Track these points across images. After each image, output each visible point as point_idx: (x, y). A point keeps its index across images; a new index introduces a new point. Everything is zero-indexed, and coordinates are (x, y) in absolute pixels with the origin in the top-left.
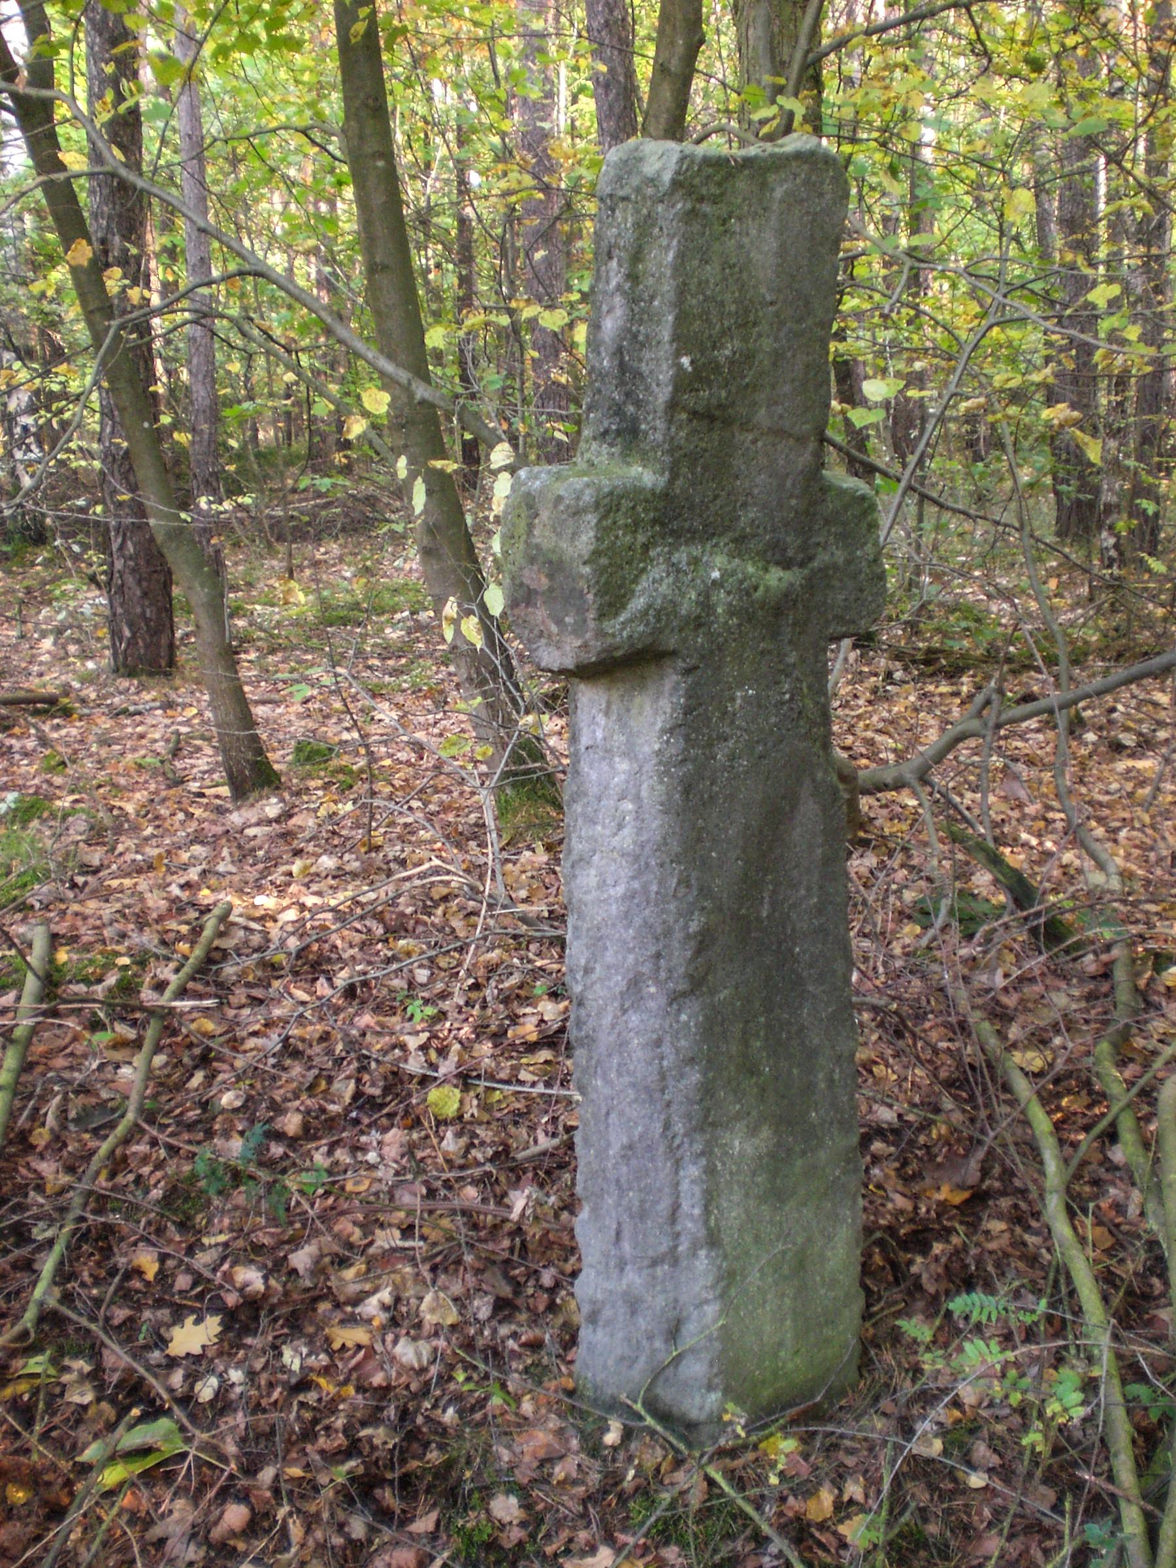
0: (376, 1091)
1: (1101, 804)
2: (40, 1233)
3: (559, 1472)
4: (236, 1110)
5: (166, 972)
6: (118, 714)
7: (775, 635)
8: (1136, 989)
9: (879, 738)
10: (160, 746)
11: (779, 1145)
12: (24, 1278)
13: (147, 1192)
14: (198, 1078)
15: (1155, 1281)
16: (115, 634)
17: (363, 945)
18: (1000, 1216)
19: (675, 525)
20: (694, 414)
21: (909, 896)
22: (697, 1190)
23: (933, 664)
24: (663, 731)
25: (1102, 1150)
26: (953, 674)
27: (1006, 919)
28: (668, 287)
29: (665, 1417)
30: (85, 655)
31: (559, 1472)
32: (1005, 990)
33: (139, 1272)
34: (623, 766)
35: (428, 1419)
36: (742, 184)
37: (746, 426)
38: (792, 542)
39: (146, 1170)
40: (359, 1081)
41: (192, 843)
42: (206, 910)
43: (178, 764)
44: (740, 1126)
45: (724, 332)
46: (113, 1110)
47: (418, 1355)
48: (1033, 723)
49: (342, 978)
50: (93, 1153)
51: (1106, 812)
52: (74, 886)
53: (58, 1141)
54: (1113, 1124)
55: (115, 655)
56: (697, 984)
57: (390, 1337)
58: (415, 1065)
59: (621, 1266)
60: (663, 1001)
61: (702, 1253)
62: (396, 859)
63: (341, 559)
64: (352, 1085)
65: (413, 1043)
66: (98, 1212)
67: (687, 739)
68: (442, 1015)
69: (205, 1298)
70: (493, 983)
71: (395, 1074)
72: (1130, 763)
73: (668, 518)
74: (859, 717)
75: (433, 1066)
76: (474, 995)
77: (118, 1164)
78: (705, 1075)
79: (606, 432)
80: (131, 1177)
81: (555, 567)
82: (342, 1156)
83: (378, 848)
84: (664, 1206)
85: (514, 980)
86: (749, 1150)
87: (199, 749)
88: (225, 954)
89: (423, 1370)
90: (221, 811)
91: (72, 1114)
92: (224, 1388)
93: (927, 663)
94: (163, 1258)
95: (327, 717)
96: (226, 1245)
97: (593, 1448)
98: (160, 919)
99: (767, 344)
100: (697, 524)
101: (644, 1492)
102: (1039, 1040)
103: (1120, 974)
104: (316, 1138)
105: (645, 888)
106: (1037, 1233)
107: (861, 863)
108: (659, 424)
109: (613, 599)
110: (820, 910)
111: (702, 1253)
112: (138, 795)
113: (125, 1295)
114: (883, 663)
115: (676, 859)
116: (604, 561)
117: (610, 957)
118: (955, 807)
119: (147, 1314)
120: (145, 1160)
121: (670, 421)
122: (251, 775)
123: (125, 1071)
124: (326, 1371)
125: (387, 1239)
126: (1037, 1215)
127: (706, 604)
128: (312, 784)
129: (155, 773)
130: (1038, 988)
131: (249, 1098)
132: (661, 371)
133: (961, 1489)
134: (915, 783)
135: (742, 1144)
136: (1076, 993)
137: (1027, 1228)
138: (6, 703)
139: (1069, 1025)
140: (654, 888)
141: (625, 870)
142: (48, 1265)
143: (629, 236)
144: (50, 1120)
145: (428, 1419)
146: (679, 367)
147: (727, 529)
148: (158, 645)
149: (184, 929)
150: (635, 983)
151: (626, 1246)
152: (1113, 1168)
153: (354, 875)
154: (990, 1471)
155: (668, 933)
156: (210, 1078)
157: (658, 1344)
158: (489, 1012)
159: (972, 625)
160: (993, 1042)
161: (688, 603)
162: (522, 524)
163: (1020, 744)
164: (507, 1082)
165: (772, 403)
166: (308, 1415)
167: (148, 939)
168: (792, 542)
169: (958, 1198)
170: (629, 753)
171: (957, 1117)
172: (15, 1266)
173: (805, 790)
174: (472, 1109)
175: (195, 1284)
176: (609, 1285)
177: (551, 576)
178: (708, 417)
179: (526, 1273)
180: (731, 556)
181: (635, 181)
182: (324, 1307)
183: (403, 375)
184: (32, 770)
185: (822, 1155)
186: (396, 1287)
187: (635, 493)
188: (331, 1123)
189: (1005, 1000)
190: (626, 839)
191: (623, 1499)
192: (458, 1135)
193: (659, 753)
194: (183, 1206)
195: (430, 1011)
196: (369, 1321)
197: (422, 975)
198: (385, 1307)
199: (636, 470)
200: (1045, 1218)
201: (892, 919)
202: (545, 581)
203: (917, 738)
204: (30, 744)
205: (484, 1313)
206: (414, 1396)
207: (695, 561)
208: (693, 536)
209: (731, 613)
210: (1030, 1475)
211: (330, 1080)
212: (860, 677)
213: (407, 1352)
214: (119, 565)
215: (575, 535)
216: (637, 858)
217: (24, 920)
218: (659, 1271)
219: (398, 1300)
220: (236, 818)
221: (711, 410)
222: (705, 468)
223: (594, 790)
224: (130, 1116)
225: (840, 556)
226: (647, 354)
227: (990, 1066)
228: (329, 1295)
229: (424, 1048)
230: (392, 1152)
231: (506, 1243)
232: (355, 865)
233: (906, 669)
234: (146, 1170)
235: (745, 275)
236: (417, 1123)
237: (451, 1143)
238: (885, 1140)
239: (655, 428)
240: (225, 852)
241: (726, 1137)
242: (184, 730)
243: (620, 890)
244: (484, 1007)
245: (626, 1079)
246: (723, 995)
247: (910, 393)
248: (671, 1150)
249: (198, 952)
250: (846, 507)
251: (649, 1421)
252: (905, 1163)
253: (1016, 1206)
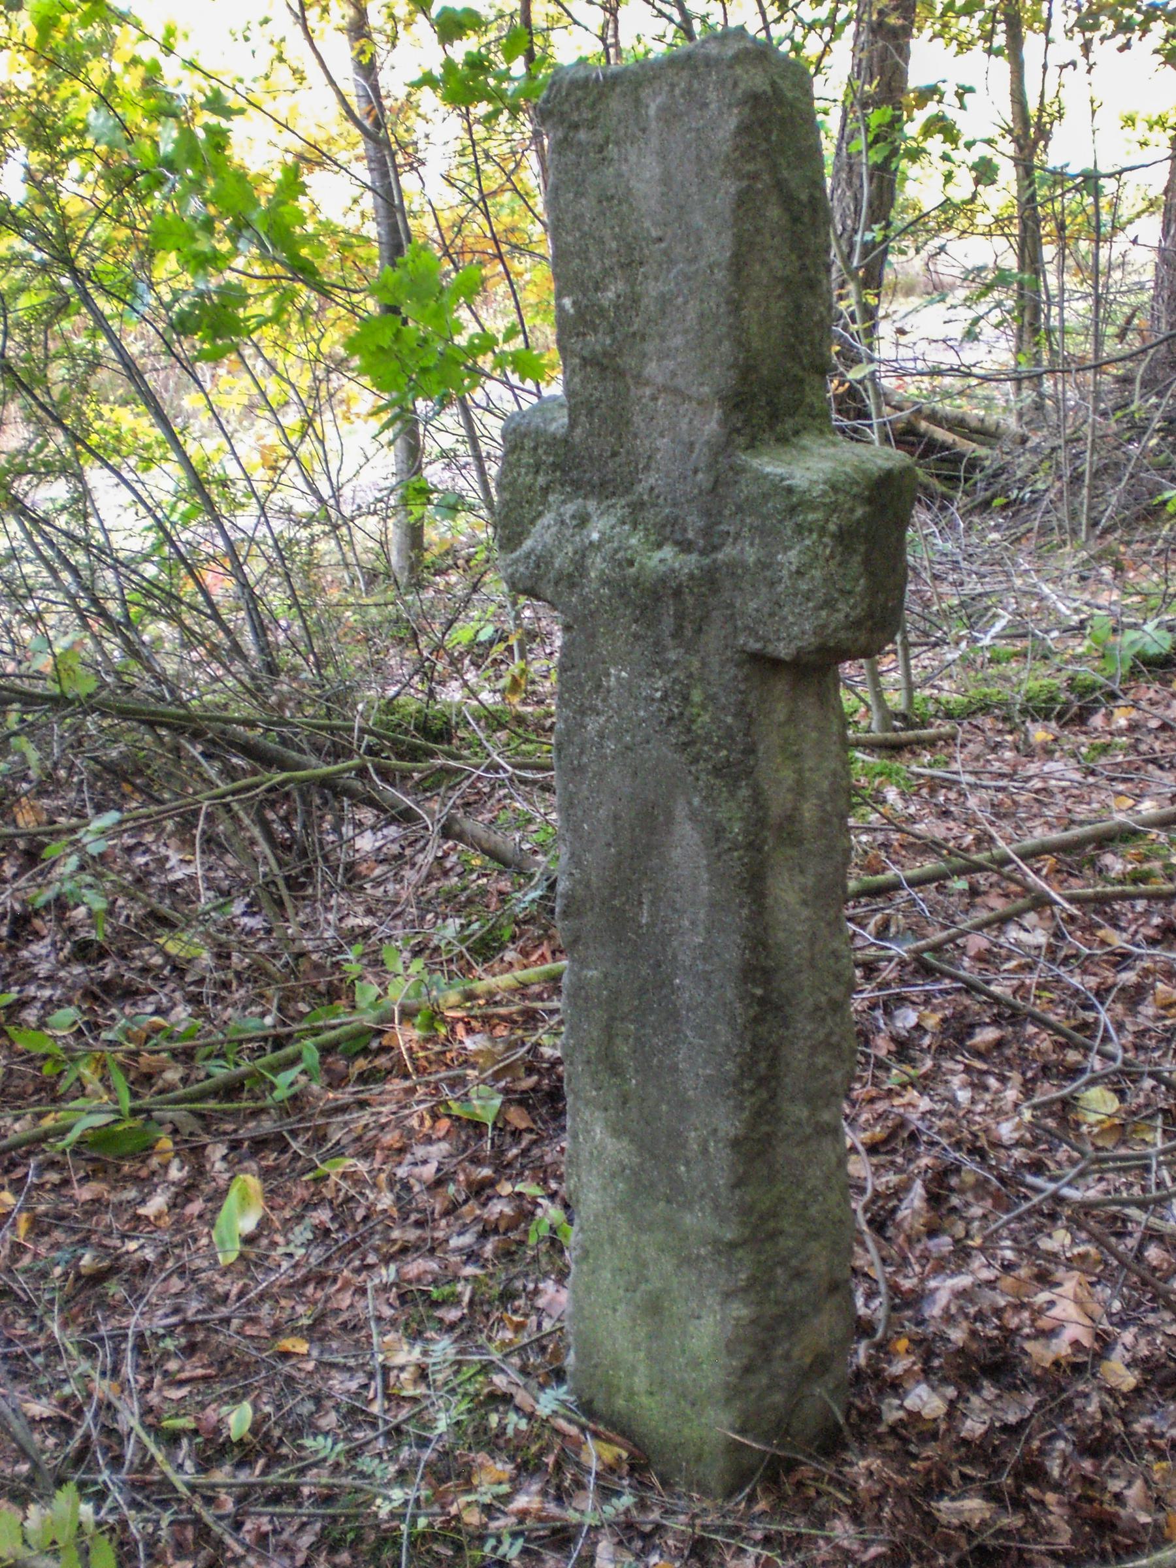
19: (575, 474)
36: (616, 104)
45: (607, 272)
101: (362, 1194)
222: (603, 420)
225: (751, 555)
235: (625, 207)
250: (766, 497)
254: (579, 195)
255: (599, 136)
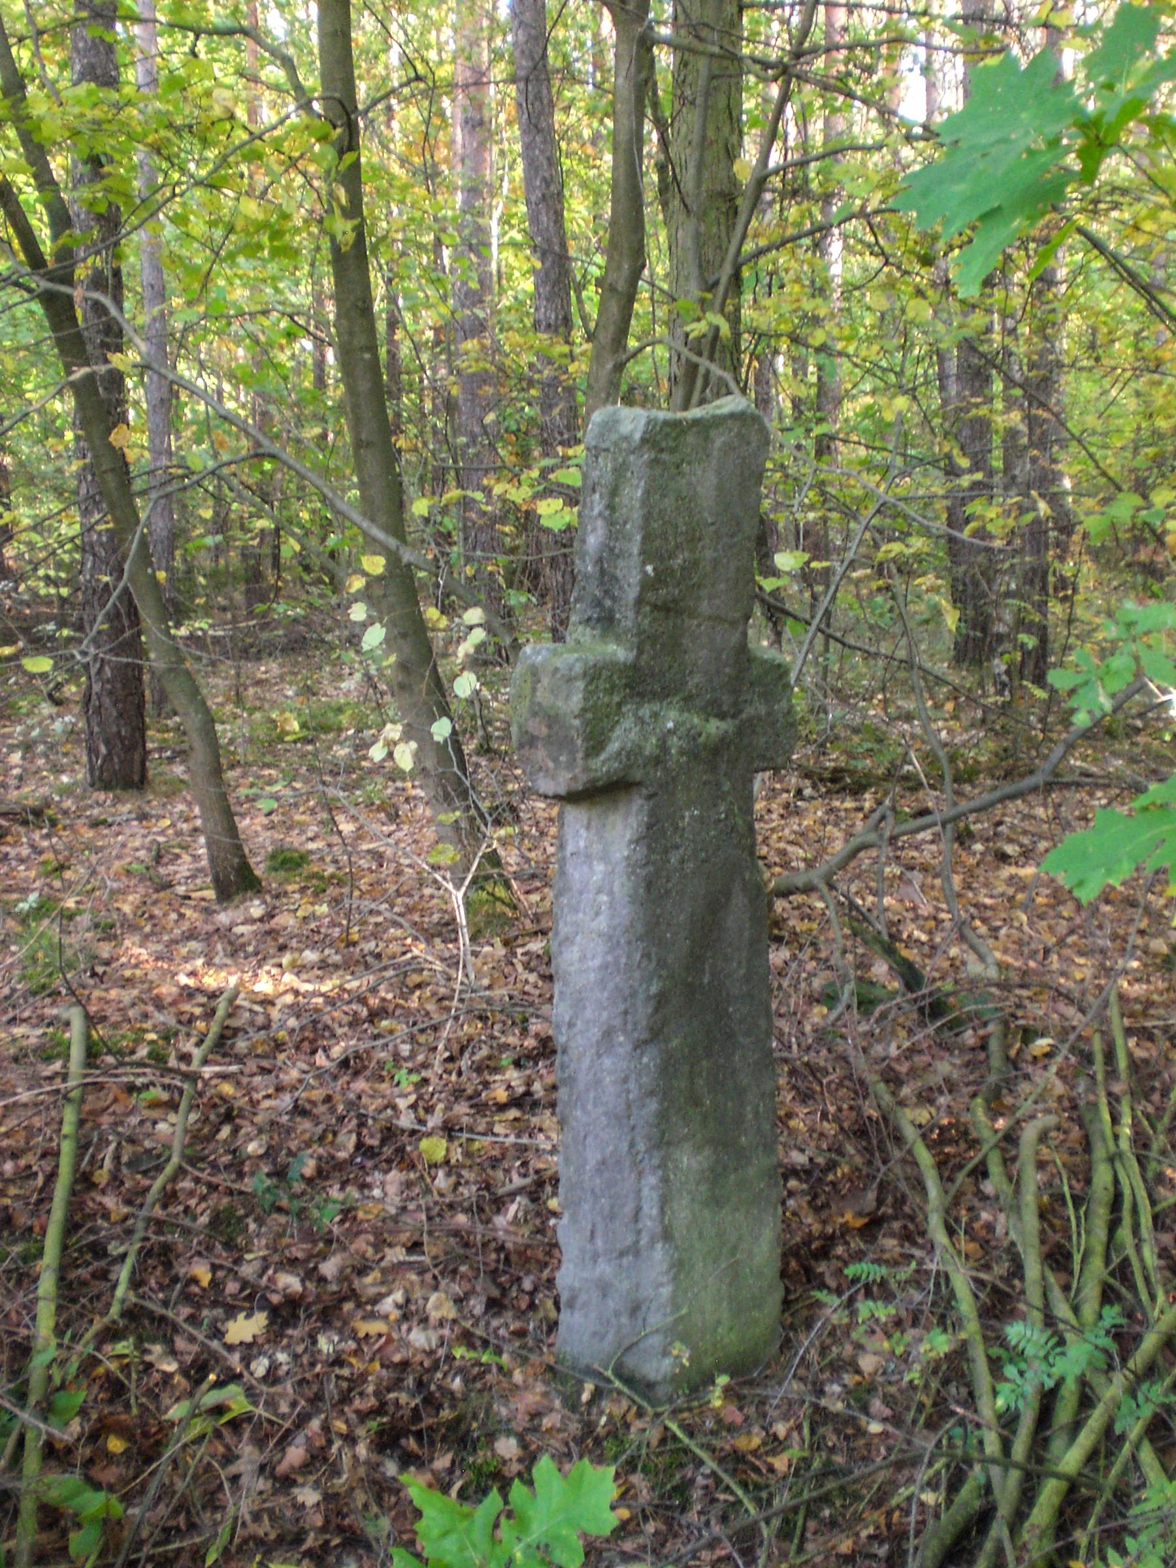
0: (375, 1142)
1: (985, 907)
2: (114, 1249)
3: (547, 1422)
4: (261, 1157)
5: (188, 1046)
6: (96, 824)
7: (714, 769)
8: (1008, 1058)
9: (790, 849)
10: (142, 854)
11: (717, 1162)
12: (104, 1286)
13: (195, 1218)
14: (225, 1132)
15: (1016, 1282)
16: (92, 751)
17: (350, 1025)
18: (893, 1235)
20: (655, 607)
21: (817, 983)
22: (655, 1195)
23: (839, 782)
24: (631, 842)
25: (976, 1184)
26: (857, 791)
27: (899, 1000)
28: (637, 515)
29: (629, 1380)
30: (58, 770)
31: (547, 1422)
32: (898, 1059)
33: (194, 1281)
34: (599, 868)
35: (439, 1387)
36: (690, 439)
37: (692, 616)
38: (726, 700)
39: (192, 1202)
40: (359, 1134)
41: (188, 939)
42: (213, 995)
43: (162, 871)
44: (687, 1146)
46: (159, 1156)
47: (429, 1340)
48: (926, 835)
49: (337, 1051)
50: (147, 1189)
51: (989, 913)
52: (94, 974)
53: (116, 1179)
54: (983, 1162)
55: (92, 770)
56: (656, 1034)
57: (404, 1327)
58: (406, 1121)
59: (595, 1258)
60: (629, 1047)
61: (659, 1246)
62: (371, 953)
63: (282, 677)
64: (354, 1137)
65: (402, 1104)
66: (159, 1232)
67: (649, 848)
68: (425, 1081)
69: (253, 1298)
70: (467, 1055)
71: (389, 1129)
72: (1013, 870)
73: (637, 683)
74: (773, 830)
75: (422, 1122)
76: (450, 1066)
77: (169, 1197)
78: (661, 1103)
79: (589, 619)
80: (181, 1208)
81: (553, 720)
82: (353, 1192)
83: (354, 944)
84: (629, 1209)
85: (485, 1051)
86: (695, 1165)
87: (178, 856)
88: (236, 1031)
89: (431, 1353)
90: (208, 912)
91: (125, 1159)
92: (273, 1367)
93: (833, 780)
94: (214, 1268)
95: (290, 828)
96: (264, 1258)
97: (571, 1403)
98: (174, 1003)
99: (709, 554)
100: (657, 688)
102: (926, 1097)
103: (994, 1045)
104: (327, 1178)
105: (617, 961)
106: (922, 1247)
107: (778, 956)
108: (631, 614)
109: (596, 745)
110: (747, 979)
111: (659, 1246)
112: (131, 898)
113: (187, 1298)
114: (794, 780)
115: (640, 939)
116: (589, 715)
117: (588, 1014)
118: (857, 908)
119: (205, 1312)
120: (191, 1194)
121: (638, 613)
122: (235, 879)
123: (162, 1127)
124: (357, 1352)
125: (396, 1254)
126: (923, 1234)
127: (663, 746)
128: (290, 888)
129: (142, 879)
130: (926, 1058)
131: (270, 1148)
132: (632, 574)
133: (861, 1432)
134: (825, 889)
135: (689, 1161)
136: (958, 1062)
137: (914, 1244)
138: (4, 815)
139: (951, 1086)
140: (623, 960)
141: (600, 947)
142: (123, 1274)
143: (609, 477)
144: (108, 1163)
145: (439, 1387)
146: (645, 573)
147: (677, 691)
148: (132, 761)
149: (198, 1011)
150: (608, 1034)
151: (599, 1243)
152: (984, 1197)
153: (337, 967)
154: (885, 1420)
155: (634, 994)
156: (236, 1131)
157: (624, 1320)
158: (464, 1078)
159: (876, 746)
160: (887, 1099)
161: (651, 746)
162: (529, 686)
163: (915, 854)
164: (484, 1134)
165: (711, 597)
166: (345, 1385)
167: (166, 1018)
168: (726, 700)
169: (860, 1222)
170: (605, 858)
171: (858, 1160)
172: (94, 1275)
173: (737, 888)
174: (457, 1155)
175: (242, 1290)
176: (585, 1275)
177: (550, 727)
178: (667, 609)
179: (513, 1281)
180: (681, 711)
181: (614, 437)
182: (348, 1306)
183: (392, 542)
184: (33, 874)
185: (751, 1171)
186: (406, 1291)
187: (612, 665)
188: (340, 1166)
189: (897, 1067)
190: (602, 923)
191: (598, 1441)
192: (448, 1175)
193: (628, 858)
194: (225, 1230)
195: (415, 1078)
196: (386, 1317)
197: (405, 1049)
198: (398, 1306)
199: (612, 647)
200: (929, 1235)
201: (805, 992)
202: (545, 731)
203: (824, 850)
204: (25, 851)
205: (478, 1309)
206: (428, 1371)
207: (655, 715)
208: (654, 696)
209: (682, 752)
210: (914, 1422)
211: (335, 1134)
212: (773, 794)
213: (419, 1338)
214: (96, 688)
215: (568, 697)
216: (610, 938)
217: (54, 1004)
218: (625, 1261)
219: (408, 1301)
220: (223, 918)
221: (667, 603)
223: (577, 886)
224: (175, 1160)
225: (763, 710)
226: (621, 563)
227: (885, 1119)
228: (353, 1295)
229: (413, 1107)
230: (392, 1189)
231: (494, 1256)
232: (337, 958)
233: (814, 786)
234: (192, 1202)
236: (412, 1167)
237: (442, 1181)
238: (800, 1180)
239: (626, 617)
240: (219, 947)
241: (677, 1154)
242: (161, 839)
243: (597, 962)
244: (460, 1074)
245: (601, 1110)
246: (675, 1043)
247: (814, 565)
248: (635, 1164)
249: (215, 1029)
251: (618, 1384)
252: (815, 1197)
253: (905, 1227)
254: (664, 496)
255: (677, 458)
